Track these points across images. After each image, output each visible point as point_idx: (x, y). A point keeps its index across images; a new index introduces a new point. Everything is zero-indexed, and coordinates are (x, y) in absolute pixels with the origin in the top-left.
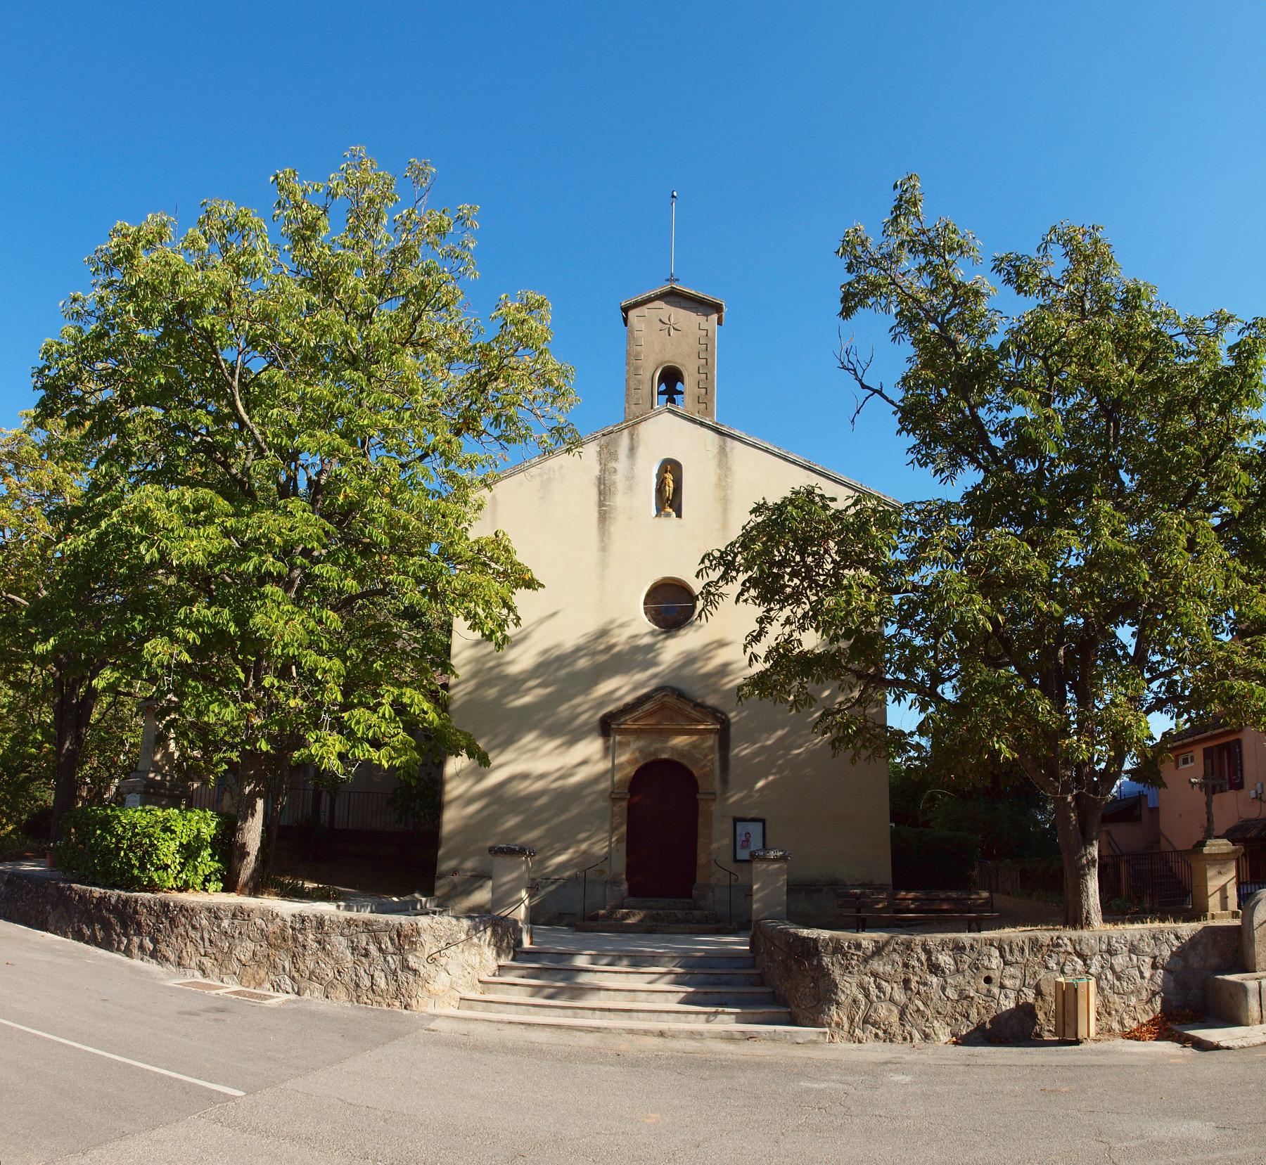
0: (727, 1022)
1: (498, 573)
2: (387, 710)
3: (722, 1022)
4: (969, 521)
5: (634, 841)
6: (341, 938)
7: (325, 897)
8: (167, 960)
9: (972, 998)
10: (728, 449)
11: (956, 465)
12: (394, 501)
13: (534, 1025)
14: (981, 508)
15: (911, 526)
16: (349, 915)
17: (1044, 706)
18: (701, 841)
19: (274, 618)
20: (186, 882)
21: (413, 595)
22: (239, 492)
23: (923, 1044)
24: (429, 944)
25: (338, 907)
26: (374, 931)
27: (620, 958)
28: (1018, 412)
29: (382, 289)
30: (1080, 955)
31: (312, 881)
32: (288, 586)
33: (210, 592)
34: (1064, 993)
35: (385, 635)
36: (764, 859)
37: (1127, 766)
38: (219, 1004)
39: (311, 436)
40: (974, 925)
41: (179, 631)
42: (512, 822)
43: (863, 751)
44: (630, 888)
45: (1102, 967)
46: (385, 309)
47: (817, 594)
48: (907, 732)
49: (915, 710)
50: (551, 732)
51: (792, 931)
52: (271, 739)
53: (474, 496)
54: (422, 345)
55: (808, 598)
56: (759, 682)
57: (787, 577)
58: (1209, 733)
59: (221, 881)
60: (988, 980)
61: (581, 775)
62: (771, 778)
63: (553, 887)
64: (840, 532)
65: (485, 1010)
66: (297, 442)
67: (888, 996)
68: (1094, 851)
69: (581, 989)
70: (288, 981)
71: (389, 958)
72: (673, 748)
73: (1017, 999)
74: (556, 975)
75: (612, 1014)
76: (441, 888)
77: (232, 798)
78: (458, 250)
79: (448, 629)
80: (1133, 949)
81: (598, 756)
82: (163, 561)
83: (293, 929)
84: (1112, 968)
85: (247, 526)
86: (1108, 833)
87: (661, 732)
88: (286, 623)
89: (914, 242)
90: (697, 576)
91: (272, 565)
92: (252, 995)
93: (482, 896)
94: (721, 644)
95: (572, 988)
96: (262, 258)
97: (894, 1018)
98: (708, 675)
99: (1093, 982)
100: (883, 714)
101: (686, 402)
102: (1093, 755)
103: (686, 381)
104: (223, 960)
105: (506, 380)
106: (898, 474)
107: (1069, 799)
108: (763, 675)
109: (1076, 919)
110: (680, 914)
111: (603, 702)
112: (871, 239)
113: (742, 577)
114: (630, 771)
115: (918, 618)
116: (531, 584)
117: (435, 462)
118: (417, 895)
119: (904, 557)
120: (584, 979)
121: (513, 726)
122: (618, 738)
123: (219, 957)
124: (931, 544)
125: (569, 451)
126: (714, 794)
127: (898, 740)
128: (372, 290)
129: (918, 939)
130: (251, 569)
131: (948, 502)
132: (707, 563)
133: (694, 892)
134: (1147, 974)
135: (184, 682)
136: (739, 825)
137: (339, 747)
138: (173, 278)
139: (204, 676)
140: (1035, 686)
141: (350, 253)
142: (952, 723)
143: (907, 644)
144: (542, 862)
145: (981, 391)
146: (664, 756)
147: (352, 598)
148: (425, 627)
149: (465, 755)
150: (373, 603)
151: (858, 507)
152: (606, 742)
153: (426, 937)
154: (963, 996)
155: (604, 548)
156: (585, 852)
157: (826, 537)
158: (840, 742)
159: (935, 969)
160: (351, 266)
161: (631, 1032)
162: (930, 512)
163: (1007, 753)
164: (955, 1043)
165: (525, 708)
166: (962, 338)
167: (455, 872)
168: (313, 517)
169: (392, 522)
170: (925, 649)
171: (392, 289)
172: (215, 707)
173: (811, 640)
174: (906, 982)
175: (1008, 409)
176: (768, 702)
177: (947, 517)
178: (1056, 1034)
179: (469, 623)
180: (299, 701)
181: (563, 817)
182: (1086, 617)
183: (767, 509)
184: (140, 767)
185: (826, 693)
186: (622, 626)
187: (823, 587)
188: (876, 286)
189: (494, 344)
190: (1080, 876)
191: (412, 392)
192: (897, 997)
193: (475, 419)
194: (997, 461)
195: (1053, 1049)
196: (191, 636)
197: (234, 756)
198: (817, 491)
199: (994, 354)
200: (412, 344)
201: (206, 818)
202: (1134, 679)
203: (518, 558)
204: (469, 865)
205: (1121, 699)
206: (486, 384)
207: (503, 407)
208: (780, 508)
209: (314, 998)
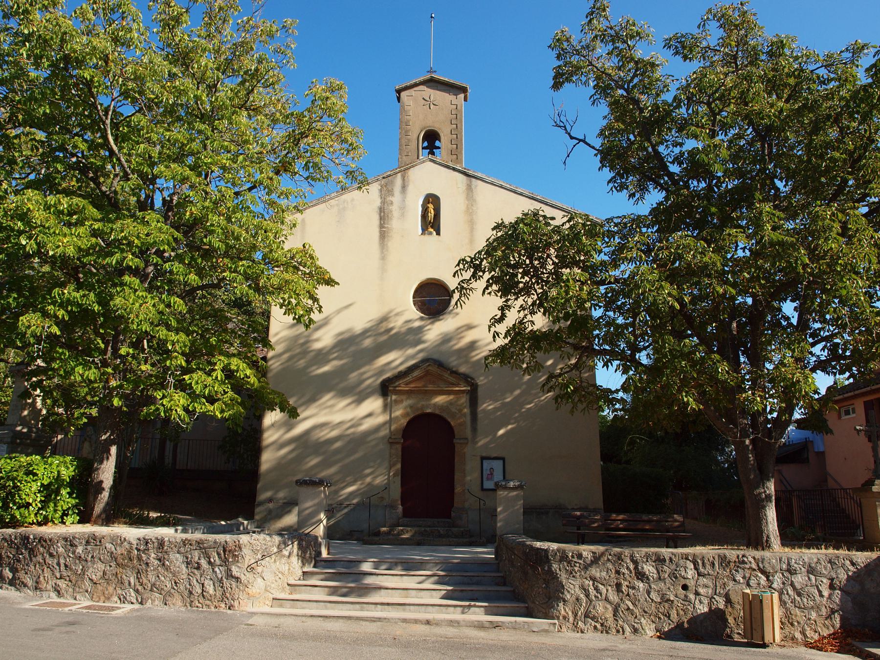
0: (478, 614)
1: (305, 274)
2: (219, 374)
3: (474, 613)
4: (655, 229)
5: (406, 475)
6: (178, 555)
7: (165, 523)
8: (25, 585)
9: (672, 601)
10: (473, 187)
11: (643, 189)
12: (229, 219)
13: (330, 617)
14: (665, 219)
15: (611, 234)
16: (184, 536)
17: (723, 368)
18: (457, 475)
19: (131, 301)
20: (46, 517)
21: (242, 288)
22: (109, 205)
23: (633, 637)
24: (248, 557)
25: (176, 531)
26: (205, 548)
27: (396, 564)
28: (690, 144)
29: (226, 67)
30: (763, 572)
31: (156, 511)
32: (143, 277)
33: (77, 279)
34: (750, 602)
35: (218, 317)
36: (506, 488)
37: (797, 416)
38: (71, 619)
39: (166, 167)
40: (671, 543)
41: (50, 308)
42: (314, 461)
43: (579, 405)
44: (404, 510)
45: (784, 583)
46: (227, 81)
47: (542, 288)
48: (613, 389)
49: (619, 373)
50: (343, 393)
51: (528, 543)
52: (122, 397)
53: (289, 218)
54: (254, 110)
55: (536, 291)
56: (501, 354)
57: (520, 276)
58: (869, 389)
59: (78, 514)
60: (685, 587)
61: (366, 425)
62: (510, 427)
63: (346, 510)
64: (558, 242)
65: (292, 607)
66: (156, 170)
67: (604, 596)
68: (771, 487)
69: (366, 588)
70: (133, 594)
71: (217, 569)
72: (435, 405)
73: (710, 605)
74: (348, 579)
75: (390, 607)
76: (260, 512)
77: (91, 446)
78: (282, 48)
79: (267, 315)
80: (811, 570)
81: (380, 410)
82: (40, 252)
83: (138, 550)
84: (792, 585)
85: (112, 229)
86: (780, 472)
87: (426, 392)
88: (141, 306)
89: (604, 35)
90: (454, 276)
91: (131, 260)
92: (101, 608)
93: (291, 519)
94: (470, 327)
95: (359, 588)
96: (136, 35)
97: (609, 615)
98: (460, 350)
99: (776, 596)
100: (594, 376)
101: (442, 154)
102: (766, 406)
103: (442, 140)
104: (76, 581)
105: (314, 137)
106: (599, 198)
107: (747, 442)
108: (503, 348)
109: (758, 541)
110: (442, 531)
111: (381, 371)
112: (573, 37)
113: (487, 276)
114: (404, 422)
115: (619, 303)
116: (330, 282)
117: (261, 193)
118: (240, 519)
119: (606, 258)
120: (369, 580)
121: (318, 389)
122: (394, 397)
123: (73, 578)
124: (627, 248)
125: (360, 188)
126: (466, 439)
127: (606, 395)
128: (218, 69)
129: (627, 552)
130: (114, 262)
131: (639, 216)
132: (461, 266)
133: (453, 514)
134: (826, 593)
135: (52, 349)
136: (485, 463)
137: (182, 401)
138: (62, 37)
139: (70, 346)
140: (714, 352)
141: (203, 41)
142: (648, 382)
143: (611, 323)
144: (336, 492)
145: (659, 134)
146: (429, 411)
147: (194, 290)
148: (250, 314)
149: (278, 410)
150: (210, 294)
151: (571, 223)
152: (385, 400)
153: (246, 551)
154: (665, 600)
155: (383, 258)
156: (369, 484)
157: (548, 245)
158: (562, 398)
159: (641, 576)
160: (204, 50)
161: (405, 621)
162: (625, 224)
163: (693, 405)
164: (659, 637)
165: (325, 374)
166: (643, 98)
167: (270, 500)
168: (165, 227)
169: (227, 233)
170: (626, 326)
171: (233, 69)
172: (79, 369)
173: (540, 322)
174: (618, 586)
175: (681, 145)
176: (507, 368)
177: (638, 226)
178: (744, 637)
179: (283, 310)
180: (149, 367)
181: (352, 458)
182: (753, 296)
183: (505, 226)
184: (8, 422)
185: (550, 362)
186: (397, 314)
187: (547, 282)
188: (578, 68)
189: (306, 113)
190: (760, 505)
191: (246, 142)
192: (611, 598)
193: (290, 164)
194: (675, 183)
195: (743, 649)
196: (61, 313)
197: (94, 412)
198: (541, 213)
199: (669, 105)
200: (247, 109)
201: (65, 462)
202: (799, 343)
203: (319, 263)
204: (281, 495)
205: (789, 360)
206: (299, 140)
207: (311, 156)
208: (514, 226)
209: (155, 606)
